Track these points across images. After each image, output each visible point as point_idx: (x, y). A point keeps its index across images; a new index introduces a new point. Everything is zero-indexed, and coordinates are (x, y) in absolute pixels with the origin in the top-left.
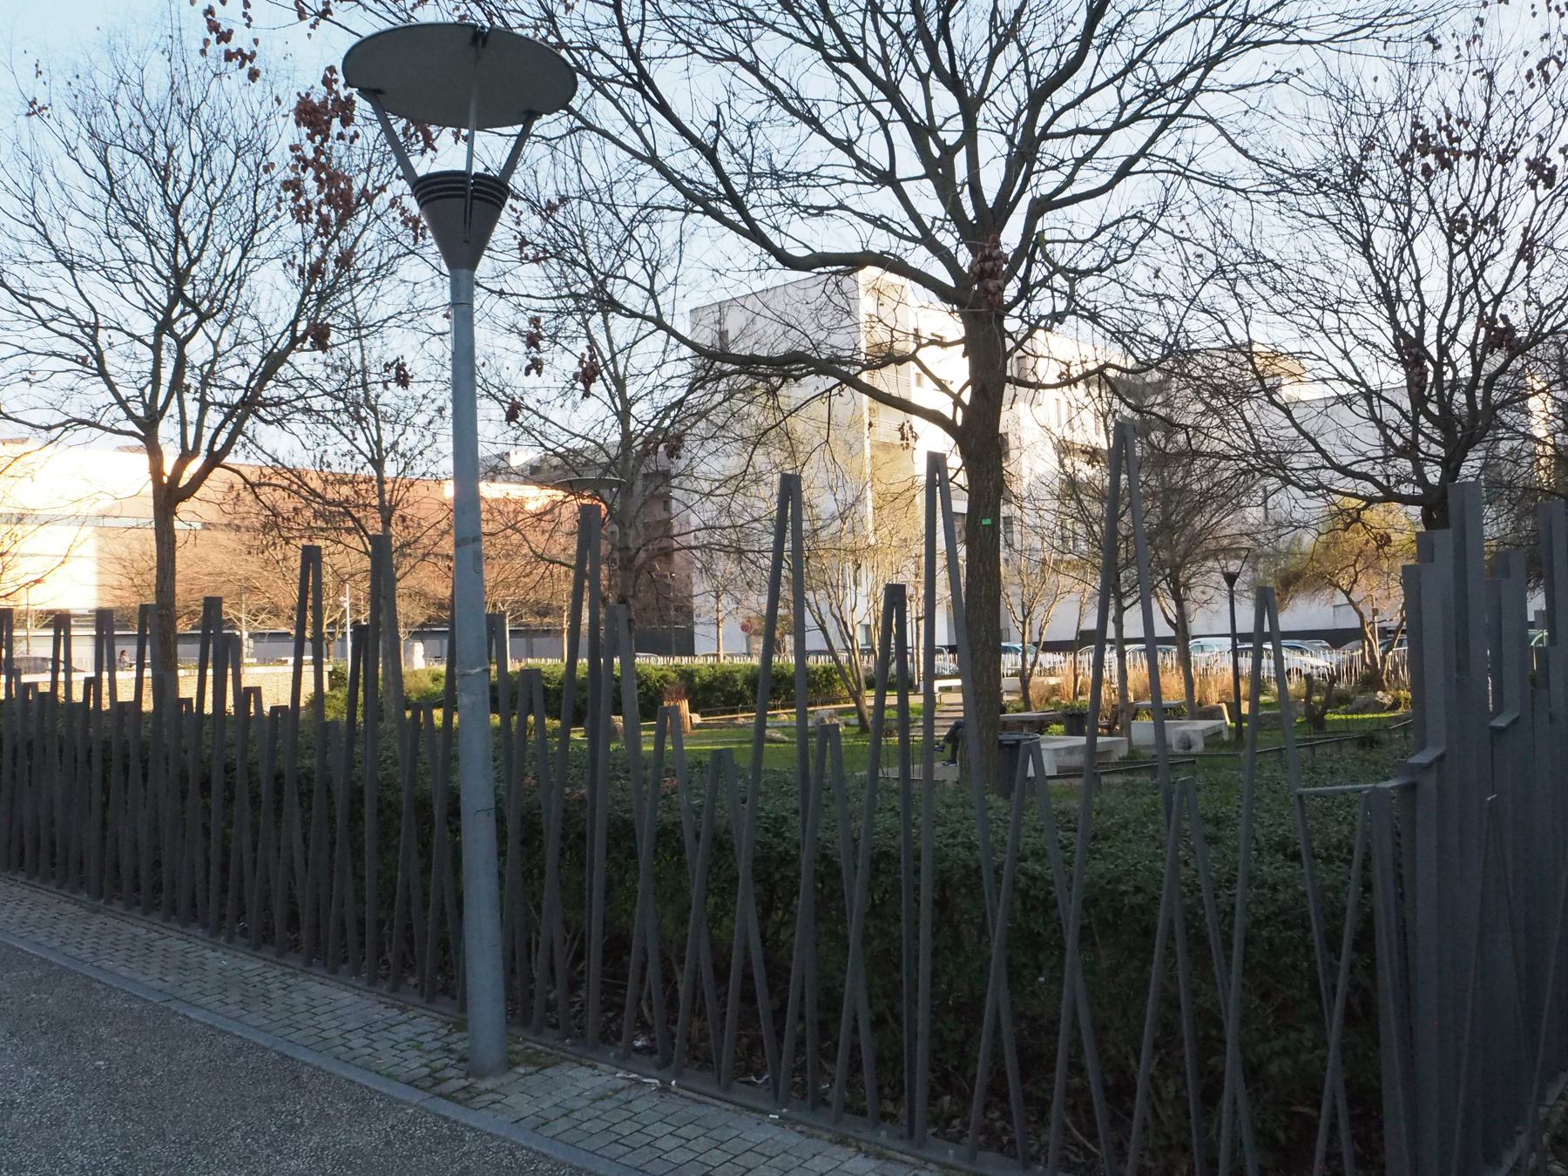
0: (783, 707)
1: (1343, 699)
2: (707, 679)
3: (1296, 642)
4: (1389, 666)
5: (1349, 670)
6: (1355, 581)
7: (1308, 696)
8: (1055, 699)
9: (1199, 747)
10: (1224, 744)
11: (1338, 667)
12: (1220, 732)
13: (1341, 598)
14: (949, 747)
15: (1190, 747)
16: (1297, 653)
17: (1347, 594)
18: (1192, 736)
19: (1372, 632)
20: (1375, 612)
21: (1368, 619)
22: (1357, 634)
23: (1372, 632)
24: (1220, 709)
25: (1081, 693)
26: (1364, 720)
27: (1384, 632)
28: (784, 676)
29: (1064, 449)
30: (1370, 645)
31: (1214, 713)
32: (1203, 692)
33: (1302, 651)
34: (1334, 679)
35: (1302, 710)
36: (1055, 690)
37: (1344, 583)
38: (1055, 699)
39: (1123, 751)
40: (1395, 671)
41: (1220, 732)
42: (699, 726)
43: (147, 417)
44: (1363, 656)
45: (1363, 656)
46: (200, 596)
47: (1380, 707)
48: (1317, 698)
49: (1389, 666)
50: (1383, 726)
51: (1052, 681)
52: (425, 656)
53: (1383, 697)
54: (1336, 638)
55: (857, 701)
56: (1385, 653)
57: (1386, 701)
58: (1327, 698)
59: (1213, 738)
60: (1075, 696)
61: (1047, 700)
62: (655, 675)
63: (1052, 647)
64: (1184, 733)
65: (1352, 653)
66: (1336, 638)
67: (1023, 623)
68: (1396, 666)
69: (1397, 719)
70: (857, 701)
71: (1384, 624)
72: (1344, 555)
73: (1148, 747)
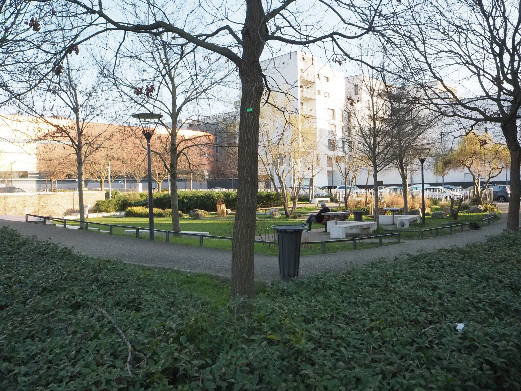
0: (261, 207)
1: (466, 207)
2: (234, 197)
3: (450, 186)
4: (484, 195)
5: (469, 197)
6: (472, 163)
7: (452, 206)
8: (359, 205)
9: (407, 226)
10: (417, 225)
11: (465, 195)
12: (416, 220)
13: (466, 170)
14: (308, 224)
15: (403, 226)
16: (450, 190)
17: (469, 168)
18: (405, 222)
19: (478, 182)
20: (479, 175)
21: (476, 178)
22: (472, 184)
23: (478, 182)
24: (418, 211)
25: (368, 204)
26: (473, 216)
27: (482, 183)
28: (262, 196)
29: (374, 118)
30: (477, 187)
31: (416, 212)
32: (413, 204)
33: (451, 189)
34: (461, 200)
35: (450, 211)
36: (359, 202)
37: (468, 164)
38: (359, 205)
39: (375, 228)
40: (486, 197)
41: (416, 220)
42: (230, 214)
43: (73, 49)
44: (474, 191)
45: (474, 191)
46: (207, 388)
47: (479, 211)
48: (456, 207)
49: (484, 195)
50: (481, 218)
51: (358, 199)
52: (142, 188)
53: (481, 207)
54: (465, 185)
55: (284, 206)
56: (482, 190)
57: (482, 208)
58: (460, 206)
59: (413, 223)
60: (366, 205)
61: (356, 206)
62: (216, 195)
63: (360, 187)
64: (401, 220)
65: (469, 190)
66: (465, 185)
67: (346, 178)
68: (486, 196)
69: (486, 216)
70: (284, 206)
71: (483, 180)
72: (467, 154)
73: (388, 225)
